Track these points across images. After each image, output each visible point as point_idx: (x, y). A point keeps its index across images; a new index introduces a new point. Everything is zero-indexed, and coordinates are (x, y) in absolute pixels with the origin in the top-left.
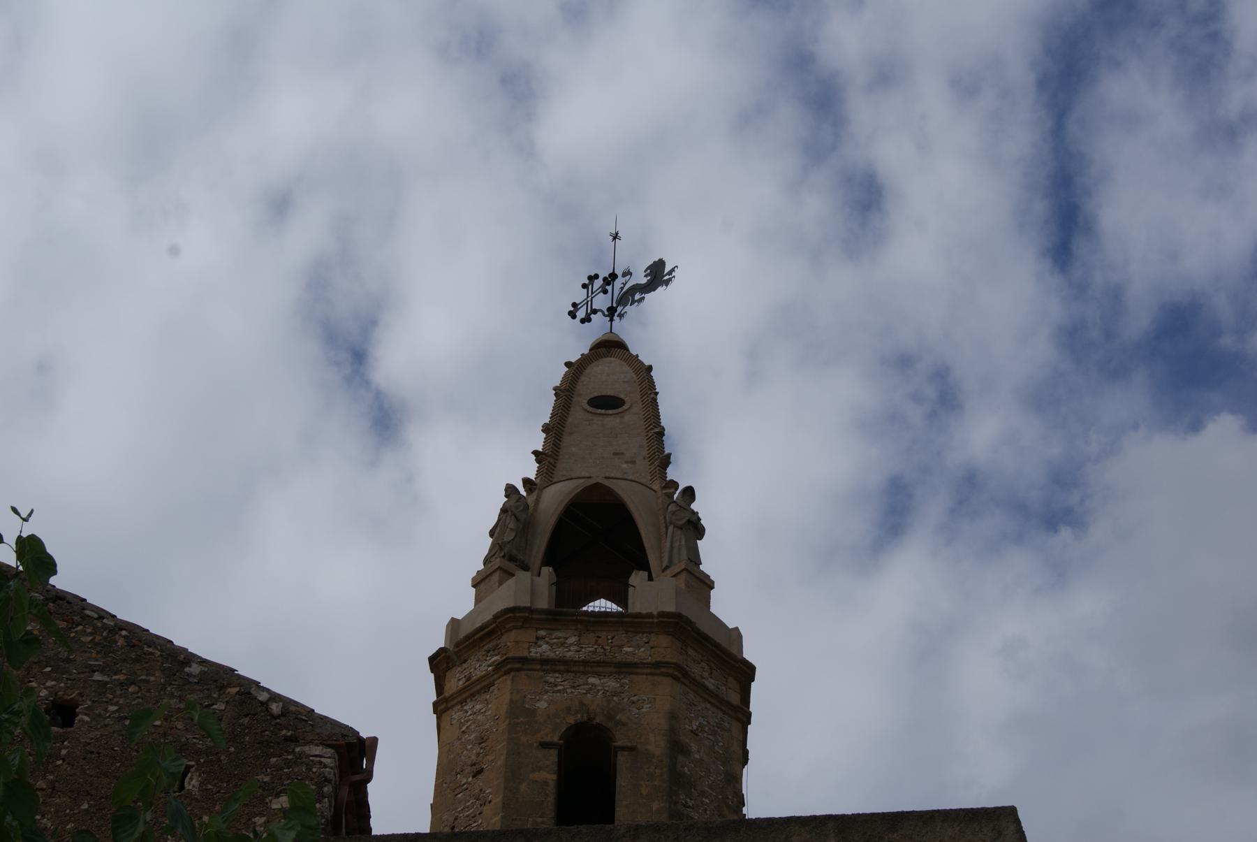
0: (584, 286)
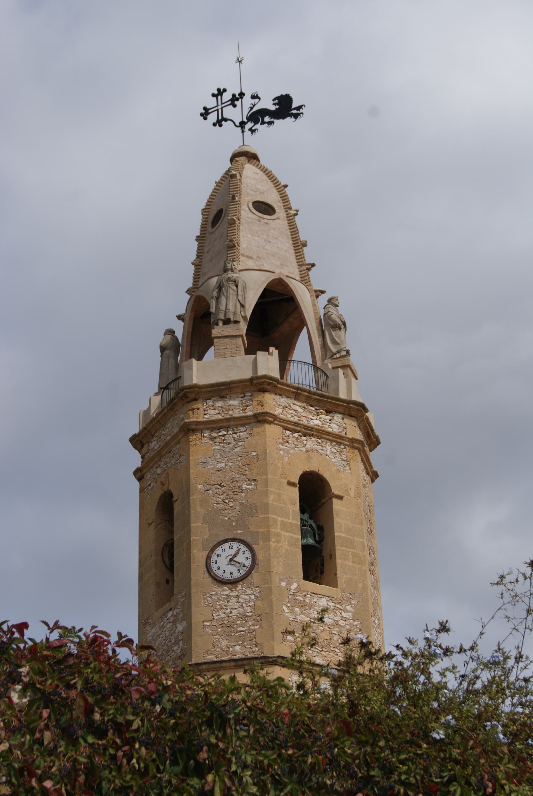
0: (213, 95)
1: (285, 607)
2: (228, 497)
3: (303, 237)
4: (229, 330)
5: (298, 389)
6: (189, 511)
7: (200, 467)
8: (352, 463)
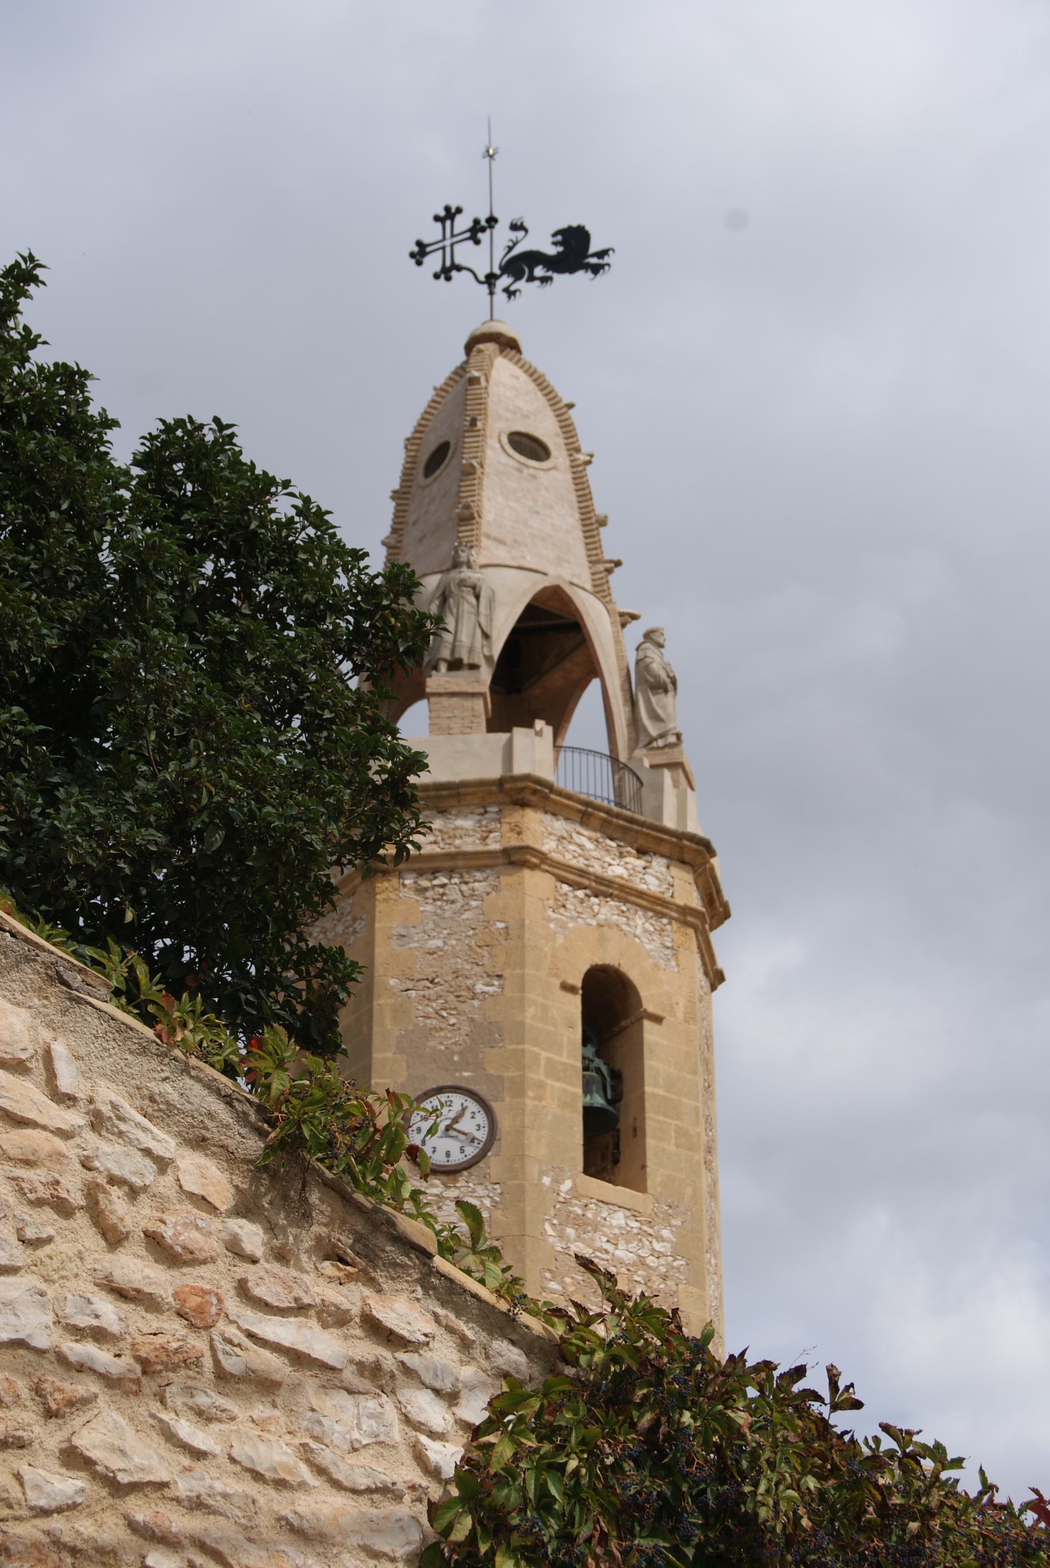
0: (437, 218)
1: (547, 1226)
2: (447, 1005)
3: (600, 508)
4: (459, 681)
5: (588, 804)
6: (370, 1028)
7: (394, 944)
8: (683, 954)
